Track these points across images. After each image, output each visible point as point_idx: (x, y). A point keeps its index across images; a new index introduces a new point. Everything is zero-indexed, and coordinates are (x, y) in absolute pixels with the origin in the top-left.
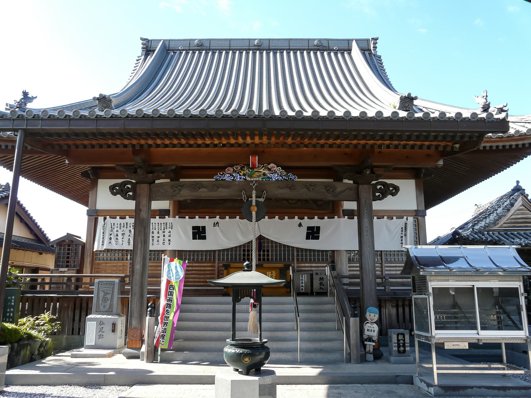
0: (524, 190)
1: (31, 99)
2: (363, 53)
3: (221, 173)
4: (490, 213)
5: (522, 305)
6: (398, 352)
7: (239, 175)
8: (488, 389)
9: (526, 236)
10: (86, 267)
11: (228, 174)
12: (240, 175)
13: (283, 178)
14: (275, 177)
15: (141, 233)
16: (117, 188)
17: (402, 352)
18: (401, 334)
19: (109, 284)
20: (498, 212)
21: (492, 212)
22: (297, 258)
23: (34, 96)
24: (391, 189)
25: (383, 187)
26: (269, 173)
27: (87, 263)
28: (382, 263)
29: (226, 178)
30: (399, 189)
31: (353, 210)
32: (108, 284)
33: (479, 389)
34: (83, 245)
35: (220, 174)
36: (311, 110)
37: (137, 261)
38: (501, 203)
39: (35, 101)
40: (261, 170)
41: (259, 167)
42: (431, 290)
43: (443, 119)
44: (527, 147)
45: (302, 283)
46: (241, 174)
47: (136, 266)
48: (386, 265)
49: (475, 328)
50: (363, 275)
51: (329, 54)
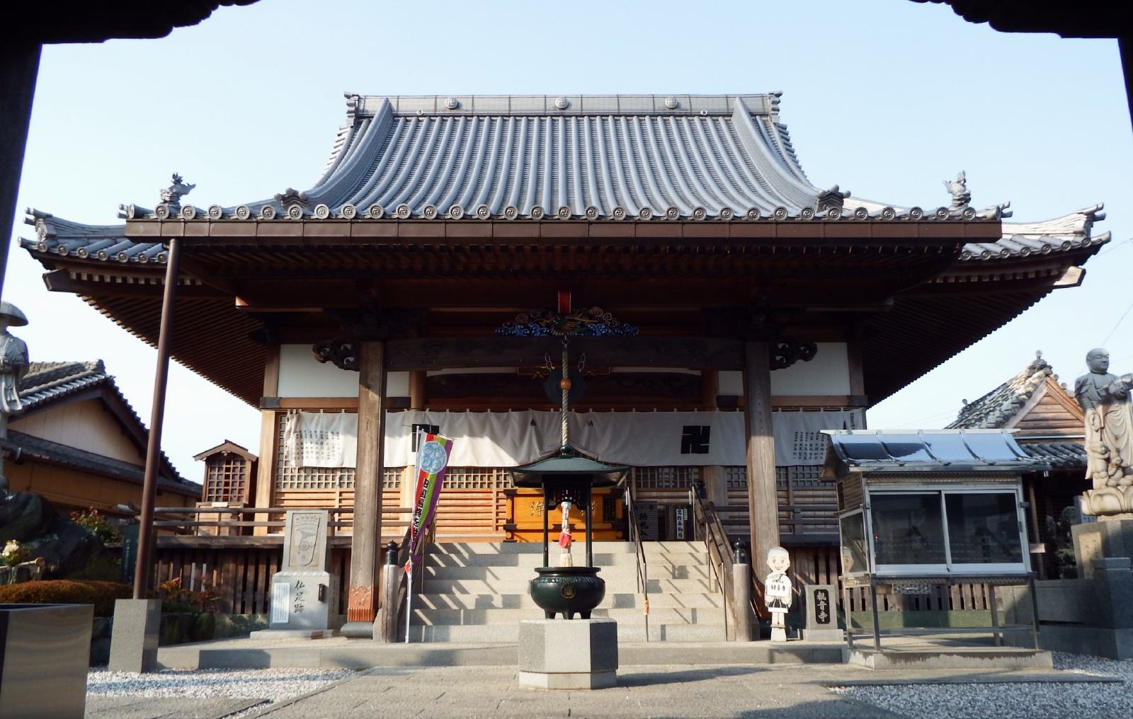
0: (1051, 368)
1: (186, 190)
3: (508, 324)
4: (988, 410)
5: (1020, 523)
7: (539, 326)
8: (964, 657)
10: (261, 500)
12: (541, 327)
13: (614, 331)
14: (602, 329)
15: (371, 426)
16: (328, 350)
17: (823, 621)
18: (822, 591)
19: (312, 518)
20: (1003, 408)
21: (992, 409)
22: (636, 483)
23: (191, 184)
24: (802, 348)
25: (787, 346)
26: (591, 323)
28: (787, 491)
29: (517, 332)
31: (736, 397)
32: (310, 519)
33: (949, 657)
34: (254, 460)
35: (506, 325)
36: (665, 207)
37: (364, 473)
38: (1007, 393)
39: (192, 192)
40: (577, 318)
41: (573, 312)
44: (1044, 277)
45: (680, 524)
47: (362, 482)
48: (796, 493)
49: (944, 562)
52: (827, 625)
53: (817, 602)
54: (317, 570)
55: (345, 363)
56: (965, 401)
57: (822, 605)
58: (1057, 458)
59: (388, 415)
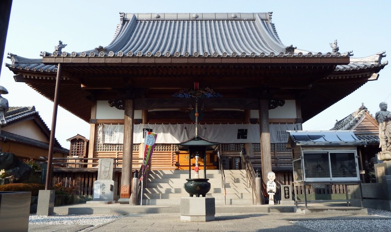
1: (64, 46)
2: (263, 22)
4: (345, 124)
6: (285, 198)
7: (187, 94)
8: (336, 210)
9: (368, 138)
11: (181, 94)
12: (188, 94)
13: (214, 96)
14: (209, 95)
17: (287, 197)
18: (287, 187)
20: (350, 123)
21: (346, 123)
22: (222, 149)
23: (65, 44)
24: (280, 102)
25: (274, 101)
26: (206, 93)
27: (90, 152)
28: (275, 152)
30: (285, 102)
31: (257, 119)
34: (88, 141)
35: (176, 94)
36: (232, 52)
37: (126, 146)
38: (352, 117)
39: (66, 47)
40: (201, 91)
41: (199, 89)
42: (303, 155)
43: (310, 57)
46: (189, 93)
48: (278, 153)
49: (329, 177)
50: (263, 179)
51: (241, 23)
52: (288, 199)
53: (285, 191)
54: (110, 180)
55: (119, 107)
56: (337, 120)
57: (287, 192)
58: (369, 141)
59: (135, 125)
